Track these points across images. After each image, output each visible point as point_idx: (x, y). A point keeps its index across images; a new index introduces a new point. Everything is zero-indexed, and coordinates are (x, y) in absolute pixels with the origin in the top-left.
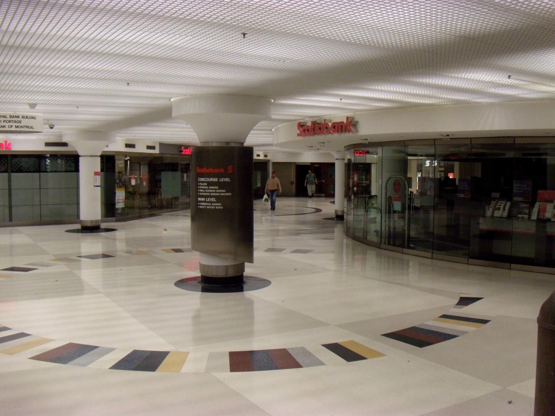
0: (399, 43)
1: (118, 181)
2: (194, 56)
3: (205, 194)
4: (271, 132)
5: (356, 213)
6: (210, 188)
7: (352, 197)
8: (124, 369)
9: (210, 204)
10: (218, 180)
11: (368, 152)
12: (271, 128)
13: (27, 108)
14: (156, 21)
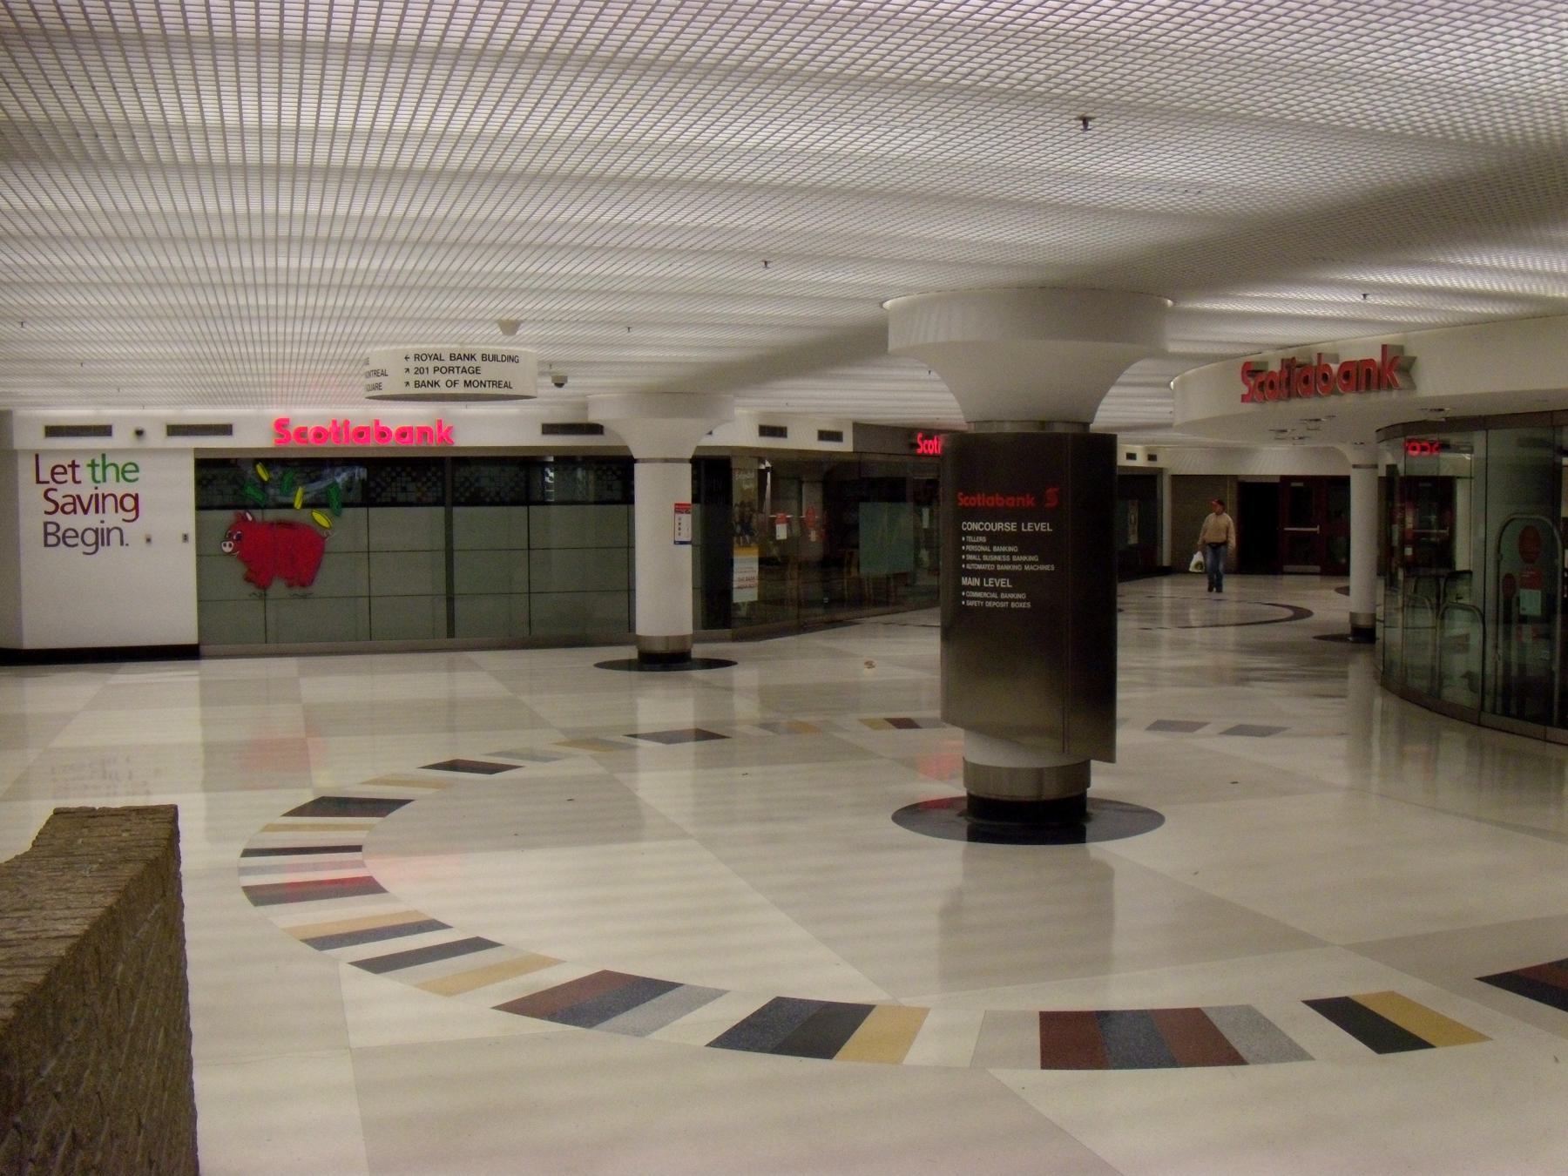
0: (1558, 128)
1: (738, 529)
2: (945, 183)
3: (980, 567)
4: (1166, 390)
5: (1410, 621)
6: (995, 549)
7: (1401, 575)
8: (748, 1049)
9: (994, 595)
10: (1019, 527)
11: (1445, 446)
12: (1165, 379)
13: (495, 332)
14: (783, 87)
